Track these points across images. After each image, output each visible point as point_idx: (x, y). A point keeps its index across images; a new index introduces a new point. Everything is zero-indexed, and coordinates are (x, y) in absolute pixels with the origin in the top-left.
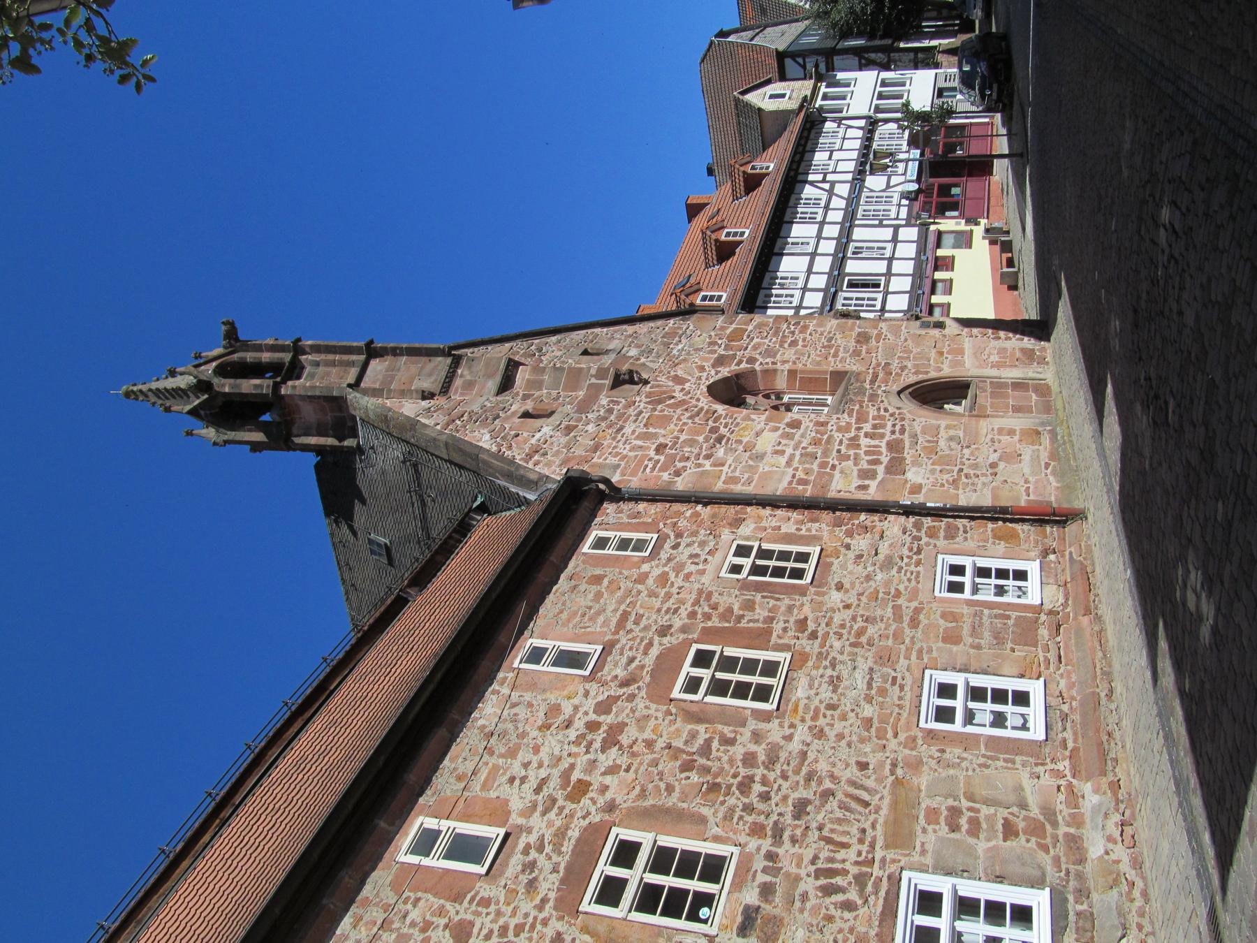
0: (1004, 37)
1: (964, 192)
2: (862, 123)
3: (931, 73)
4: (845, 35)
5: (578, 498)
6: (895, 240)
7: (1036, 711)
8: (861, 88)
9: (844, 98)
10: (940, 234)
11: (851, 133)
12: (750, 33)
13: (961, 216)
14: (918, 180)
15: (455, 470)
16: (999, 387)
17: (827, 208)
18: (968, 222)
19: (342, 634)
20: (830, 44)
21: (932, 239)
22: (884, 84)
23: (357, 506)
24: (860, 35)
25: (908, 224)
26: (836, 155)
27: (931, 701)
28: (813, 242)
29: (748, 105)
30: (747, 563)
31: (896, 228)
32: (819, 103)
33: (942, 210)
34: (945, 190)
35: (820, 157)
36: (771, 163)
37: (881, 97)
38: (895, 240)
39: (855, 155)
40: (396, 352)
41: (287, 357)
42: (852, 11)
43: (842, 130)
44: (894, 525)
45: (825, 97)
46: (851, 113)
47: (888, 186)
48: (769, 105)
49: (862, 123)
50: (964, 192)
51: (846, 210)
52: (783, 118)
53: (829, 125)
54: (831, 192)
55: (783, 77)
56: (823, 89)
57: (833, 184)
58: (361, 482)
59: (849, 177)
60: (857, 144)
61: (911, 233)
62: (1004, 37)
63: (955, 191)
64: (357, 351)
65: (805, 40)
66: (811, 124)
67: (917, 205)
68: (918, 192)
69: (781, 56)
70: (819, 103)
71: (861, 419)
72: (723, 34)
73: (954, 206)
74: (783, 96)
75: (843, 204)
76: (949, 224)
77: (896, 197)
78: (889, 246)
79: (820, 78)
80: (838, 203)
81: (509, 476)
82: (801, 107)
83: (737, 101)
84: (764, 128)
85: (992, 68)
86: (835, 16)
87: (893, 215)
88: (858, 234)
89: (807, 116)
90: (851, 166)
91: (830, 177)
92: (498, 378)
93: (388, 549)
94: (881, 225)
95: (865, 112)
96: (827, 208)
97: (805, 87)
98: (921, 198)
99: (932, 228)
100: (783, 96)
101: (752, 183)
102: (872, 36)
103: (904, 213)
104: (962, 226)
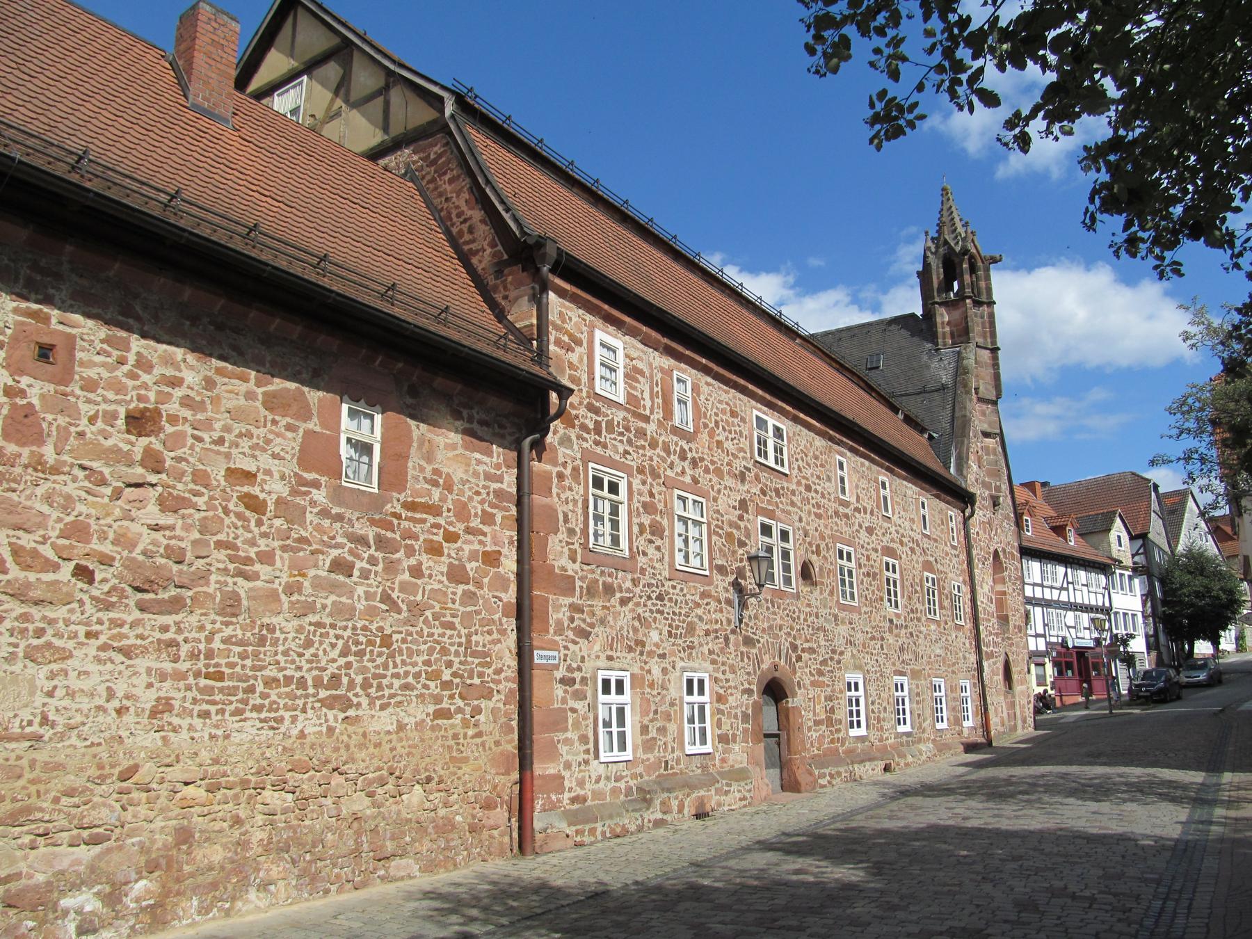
1: (1070, 679)
2: (1107, 604)
3: (1144, 649)
5: (963, 498)
6: (1037, 636)
7: (616, 755)
8: (1129, 600)
9: (1122, 589)
10: (1043, 665)
11: (1100, 597)
12: (1157, 509)
13: (1056, 679)
14: (1074, 647)
15: (948, 419)
16: (1012, 705)
17: (1052, 587)
18: (1052, 683)
20: (1156, 572)
21: (1039, 660)
22: (1133, 615)
24: (1164, 593)
25: (1047, 644)
26: (1085, 589)
27: (613, 676)
28: (1031, 581)
29: (1112, 521)
30: (956, 592)
31: (1044, 636)
32: (1118, 571)
33: (1056, 664)
34: (1069, 666)
35: (1082, 575)
36: (1073, 542)
37: (1125, 614)
38: (1037, 636)
39: (1086, 602)
41: (984, 298)
43: (1102, 591)
44: (973, 658)
45: (1121, 575)
46: (1113, 595)
47: (1068, 627)
48: (1113, 535)
49: (1107, 604)
50: (1070, 679)
51: (1052, 600)
54: (1061, 589)
55: (1132, 538)
56: (1127, 573)
57: (1067, 589)
59: (1072, 600)
60: (1093, 603)
61: (1042, 647)
63: (1070, 672)
64: (994, 342)
65: (1156, 551)
67: (1059, 648)
68: (1067, 648)
69: (1143, 536)
70: (1118, 571)
71: (997, 634)
72: (1156, 487)
73: (1060, 673)
74: (1120, 545)
75: (1055, 598)
76: (1050, 670)
77: (1062, 633)
78: (1033, 632)
79: (1135, 570)
80: (1055, 595)
82: (1116, 560)
83: (1114, 513)
87: (1052, 633)
88: (1038, 610)
89: (1109, 566)
90: (1079, 601)
91: (1071, 586)
92: (989, 430)
93: (878, 368)
94: (1045, 625)
95: (1114, 605)
96: (1052, 587)
97: (1128, 562)
98: (1064, 650)
99: (1047, 660)
100: (1120, 545)
101: (1059, 530)
102: (1165, 602)
103: (1054, 640)
104: (1049, 680)
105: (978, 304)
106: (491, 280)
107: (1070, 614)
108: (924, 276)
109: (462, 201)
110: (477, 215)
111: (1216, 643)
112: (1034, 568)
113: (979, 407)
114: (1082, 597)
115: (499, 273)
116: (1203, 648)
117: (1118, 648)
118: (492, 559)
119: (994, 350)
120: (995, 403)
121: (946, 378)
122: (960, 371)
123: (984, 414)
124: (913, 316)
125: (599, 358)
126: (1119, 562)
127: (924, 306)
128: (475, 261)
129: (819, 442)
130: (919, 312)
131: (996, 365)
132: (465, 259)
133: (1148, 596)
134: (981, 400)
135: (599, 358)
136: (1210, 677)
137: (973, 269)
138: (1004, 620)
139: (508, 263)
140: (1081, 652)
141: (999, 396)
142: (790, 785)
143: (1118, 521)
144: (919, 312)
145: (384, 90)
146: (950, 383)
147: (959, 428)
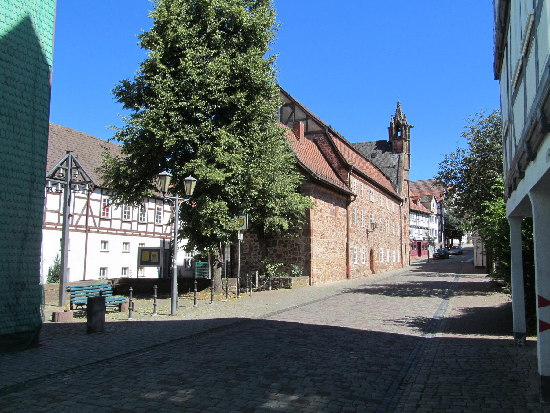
0: (448, 258)
4: (445, 218)
5: (398, 200)
8: (435, 225)
15: (396, 176)
19: (351, 141)
23: (381, 151)
24: (445, 222)
34: (415, 246)
35: (421, 218)
40: (409, 159)
42: (451, 220)
44: (400, 245)
48: (432, 204)
52: (428, 207)
53: (427, 219)
58: (386, 153)
62: (448, 258)
64: (409, 152)
66: (427, 215)
73: (412, 249)
79: (437, 215)
81: (399, 189)
83: (433, 195)
84: (426, 203)
85: (443, 255)
86: (450, 216)
97: (436, 212)
102: (445, 225)
103: (411, 238)
105: (406, 141)
106: (337, 170)
107: (417, 230)
108: (390, 129)
109: (329, 151)
110: (333, 155)
111: (460, 240)
112: (414, 217)
113: (404, 172)
114: (421, 224)
115: (339, 169)
116: (456, 242)
117: (431, 242)
118: (344, 227)
119: (409, 155)
120: (408, 171)
121: (396, 163)
122: (399, 161)
123: (405, 174)
124: (386, 141)
125: (356, 185)
126: (432, 213)
127: (389, 138)
128: (333, 165)
129: (378, 193)
130: (388, 140)
131: (409, 159)
132: (330, 165)
133: (440, 223)
134: (405, 170)
135: (356, 185)
136: (460, 252)
137: (405, 129)
138: (405, 233)
139: (341, 168)
140: (419, 243)
141: (409, 168)
142: (373, 272)
143: (434, 198)
144: (388, 140)
145: (306, 119)
146: (397, 165)
147: (398, 179)
